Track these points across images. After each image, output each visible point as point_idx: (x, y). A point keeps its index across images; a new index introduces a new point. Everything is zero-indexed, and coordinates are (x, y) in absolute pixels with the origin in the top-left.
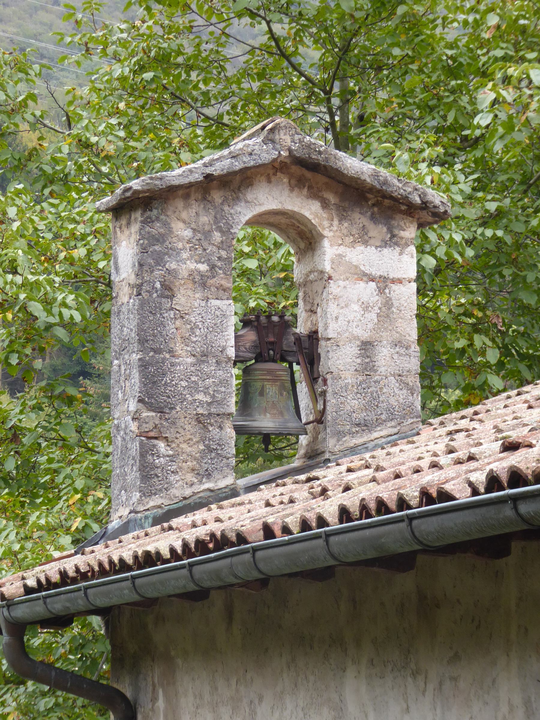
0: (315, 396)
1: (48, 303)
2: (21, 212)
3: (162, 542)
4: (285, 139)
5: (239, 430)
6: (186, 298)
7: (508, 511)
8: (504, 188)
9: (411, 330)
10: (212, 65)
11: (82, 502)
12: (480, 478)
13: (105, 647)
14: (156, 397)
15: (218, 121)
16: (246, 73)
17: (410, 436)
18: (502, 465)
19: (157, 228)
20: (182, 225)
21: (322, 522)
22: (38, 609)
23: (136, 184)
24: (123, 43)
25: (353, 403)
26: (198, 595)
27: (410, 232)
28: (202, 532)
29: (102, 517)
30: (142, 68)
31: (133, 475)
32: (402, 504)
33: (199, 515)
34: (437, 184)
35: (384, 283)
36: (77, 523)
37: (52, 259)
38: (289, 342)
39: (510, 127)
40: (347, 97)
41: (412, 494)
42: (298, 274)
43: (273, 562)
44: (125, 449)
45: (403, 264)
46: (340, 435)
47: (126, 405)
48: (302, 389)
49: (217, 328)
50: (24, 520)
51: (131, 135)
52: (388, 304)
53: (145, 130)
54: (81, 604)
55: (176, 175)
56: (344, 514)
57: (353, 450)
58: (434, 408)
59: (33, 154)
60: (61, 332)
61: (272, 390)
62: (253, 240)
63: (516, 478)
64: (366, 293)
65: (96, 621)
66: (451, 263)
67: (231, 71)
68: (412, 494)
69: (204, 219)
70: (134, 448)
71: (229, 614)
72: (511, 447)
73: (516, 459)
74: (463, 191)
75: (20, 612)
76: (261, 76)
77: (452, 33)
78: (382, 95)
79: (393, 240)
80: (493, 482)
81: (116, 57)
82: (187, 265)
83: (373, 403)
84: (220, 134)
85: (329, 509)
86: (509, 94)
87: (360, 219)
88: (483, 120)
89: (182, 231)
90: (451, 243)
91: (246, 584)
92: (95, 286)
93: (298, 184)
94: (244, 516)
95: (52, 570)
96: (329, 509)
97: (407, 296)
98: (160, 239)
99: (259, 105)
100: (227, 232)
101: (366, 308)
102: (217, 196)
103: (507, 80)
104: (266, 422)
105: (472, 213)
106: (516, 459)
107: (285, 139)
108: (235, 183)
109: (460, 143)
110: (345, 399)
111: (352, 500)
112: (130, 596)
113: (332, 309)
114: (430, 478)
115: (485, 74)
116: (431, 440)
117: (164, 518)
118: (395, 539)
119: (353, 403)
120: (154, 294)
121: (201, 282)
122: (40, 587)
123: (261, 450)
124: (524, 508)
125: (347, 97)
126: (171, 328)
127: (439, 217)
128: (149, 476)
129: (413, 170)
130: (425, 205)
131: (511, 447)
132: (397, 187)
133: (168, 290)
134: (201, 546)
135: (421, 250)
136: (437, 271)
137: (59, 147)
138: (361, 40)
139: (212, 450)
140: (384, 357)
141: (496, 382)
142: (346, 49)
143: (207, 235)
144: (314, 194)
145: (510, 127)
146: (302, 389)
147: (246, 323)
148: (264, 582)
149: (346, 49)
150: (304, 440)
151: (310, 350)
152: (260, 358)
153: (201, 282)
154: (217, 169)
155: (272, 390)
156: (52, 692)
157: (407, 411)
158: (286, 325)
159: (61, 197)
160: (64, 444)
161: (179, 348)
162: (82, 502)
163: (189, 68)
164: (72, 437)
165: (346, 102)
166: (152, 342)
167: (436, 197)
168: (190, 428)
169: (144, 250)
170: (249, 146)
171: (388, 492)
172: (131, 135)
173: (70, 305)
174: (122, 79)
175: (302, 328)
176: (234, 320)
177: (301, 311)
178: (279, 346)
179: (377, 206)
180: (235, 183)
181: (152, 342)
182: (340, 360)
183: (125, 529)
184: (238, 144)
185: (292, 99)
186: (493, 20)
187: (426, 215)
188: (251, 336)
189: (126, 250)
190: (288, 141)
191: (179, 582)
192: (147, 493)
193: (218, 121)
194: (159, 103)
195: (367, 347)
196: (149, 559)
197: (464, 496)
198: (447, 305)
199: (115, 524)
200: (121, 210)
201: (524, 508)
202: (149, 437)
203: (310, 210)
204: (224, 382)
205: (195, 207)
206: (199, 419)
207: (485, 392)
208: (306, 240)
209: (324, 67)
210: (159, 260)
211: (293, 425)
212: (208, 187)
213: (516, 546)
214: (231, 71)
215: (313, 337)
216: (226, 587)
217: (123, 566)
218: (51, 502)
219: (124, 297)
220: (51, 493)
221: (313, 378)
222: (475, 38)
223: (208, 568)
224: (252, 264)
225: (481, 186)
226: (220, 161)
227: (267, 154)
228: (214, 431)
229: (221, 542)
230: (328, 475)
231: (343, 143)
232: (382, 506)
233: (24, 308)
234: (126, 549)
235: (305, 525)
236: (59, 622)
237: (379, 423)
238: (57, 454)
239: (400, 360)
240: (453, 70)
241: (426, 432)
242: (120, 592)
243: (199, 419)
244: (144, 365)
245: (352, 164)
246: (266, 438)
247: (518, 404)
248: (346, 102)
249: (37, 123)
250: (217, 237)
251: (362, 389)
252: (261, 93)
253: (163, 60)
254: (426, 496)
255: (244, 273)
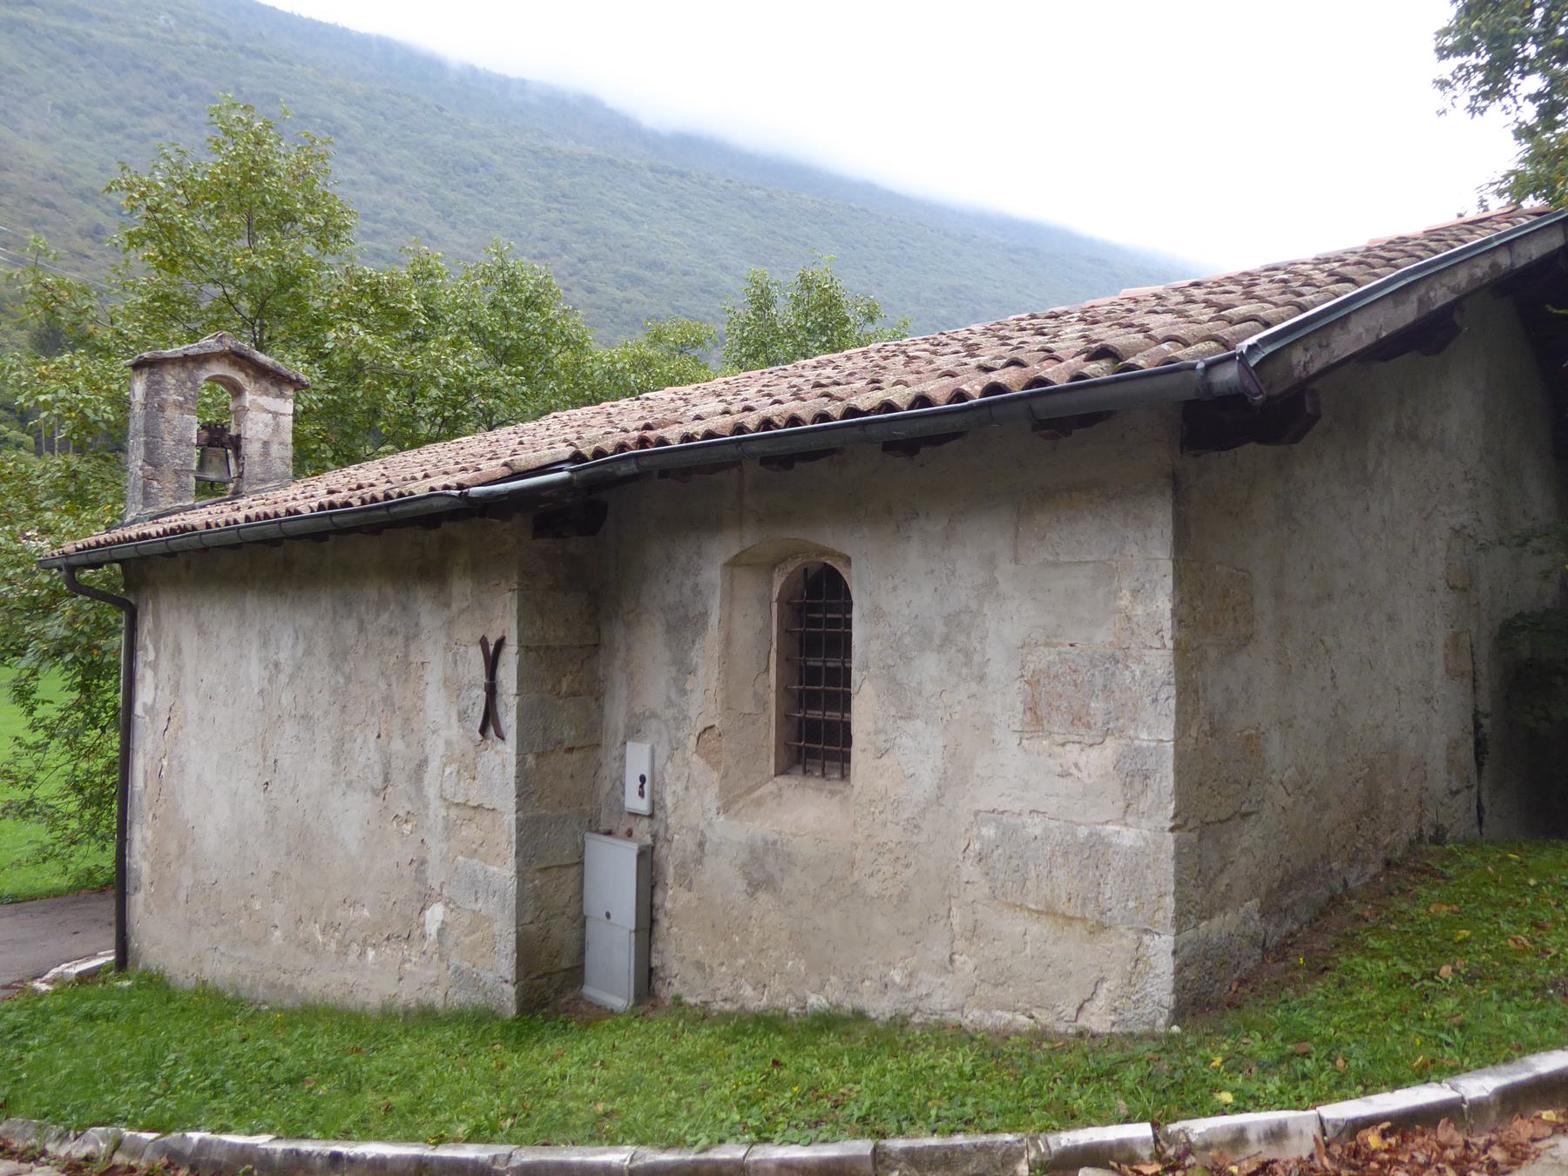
0: (238, 465)
1: (96, 411)
2: (82, 364)
3: (152, 529)
4: (228, 342)
5: (197, 479)
6: (171, 413)
7: (327, 521)
8: (338, 379)
9: (289, 438)
10: (191, 303)
11: (112, 509)
12: (315, 505)
13: (121, 580)
14: (152, 458)
15: (195, 331)
16: (210, 309)
17: (284, 487)
18: (325, 500)
19: (157, 378)
20: (170, 378)
21: (236, 522)
22: (84, 559)
23: (146, 355)
24: (144, 287)
25: (258, 470)
26: (171, 555)
27: (290, 392)
28: (173, 525)
29: (121, 517)
30: (154, 300)
31: (139, 497)
32: (277, 515)
33: (173, 518)
34: (305, 372)
35: (276, 415)
36: (108, 519)
37: (99, 389)
38: (225, 439)
39: (342, 350)
40: (263, 327)
41: (282, 511)
42: (231, 407)
43: (210, 540)
44: (135, 484)
45: (287, 407)
46: (250, 484)
47: (136, 461)
48: (232, 462)
49: (188, 428)
50: (78, 516)
51: (146, 332)
52: (278, 425)
53: (154, 331)
54: (107, 557)
55: (168, 352)
56: (247, 519)
57: (257, 492)
58: (296, 476)
59: (90, 336)
60: (102, 425)
61: (215, 461)
62: (210, 389)
63: (332, 505)
64: (266, 419)
65: (117, 566)
66: (311, 410)
67: (203, 307)
68: (282, 511)
69: (183, 375)
70: (140, 484)
71: (188, 568)
72: (331, 492)
73: (332, 498)
74: (1032, 709)
75: (73, 561)
76: (219, 311)
77: (318, 304)
78: (281, 329)
79: (281, 395)
80: (321, 507)
81: (140, 294)
82: (173, 397)
83: (268, 470)
84: (194, 336)
85: (240, 516)
86: (342, 335)
87: (265, 384)
88: (330, 345)
89: (170, 380)
90: (311, 400)
91: (196, 550)
92: (122, 403)
93: (233, 364)
94: (196, 518)
95: (92, 541)
96: (240, 516)
97: (287, 421)
98: (158, 383)
99: (216, 324)
100: (194, 382)
101: (266, 426)
102: (190, 365)
103: (342, 329)
104: (212, 476)
105: (323, 387)
106: (332, 498)
107: (228, 342)
108: (201, 360)
109: (318, 355)
110: (253, 467)
111: (252, 513)
112: (133, 554)
113: (249, 425)
114: (292, 504)
115: (331, 325)
116: (296, 489)
117: (155, 518)
118: (272, 531)
119: (258, 470)
120: (155, 409)
121: (180, 406)
122: (85, 548)
123: (208, 490)
124: (335, 519)
125: (263, 327)
126: (162, 427)
127: (305, 387)
128: (147, 498)
129: (295, 364)
130: (298, 381)
131: (331, 492)
132: (284, 370)
133: (161, 408)
134: (173, 531)
135: (296, 402)
136: (304, 413)
137: (104, 334)
138: (271, 301)
139: (182, 487)
140: (275, 449)
141: (330, 465)
142: (263, 305)
143: (184, 383)
144: (242, 369)
145: (342, 350)
146: (232, 462)
147: (203, 427)
148: (206, 549)
149: (263, 305)
150: (231, 486)
151: (236, 443)
152: (210, 445)
153: (180, 406)
154: (190, 352)
155: (215, 461)
156: (91, 601)
157: (285, 475)
158: (224, 430)
159: (107, 358)
160: (103, 481)
161: (166, 437)
162: (112, 509)
163: (180, 303)
164: (108, 477)
165: (262, 330)
166: (151, 432)
167: (304, 378)
168: (170, 476)
169: (149, 387)
170: (208, 342)
171: (269, 510)
172: (146, 332)
173: (109, 413)
174: (143, 304)
175: (233, 432)
176: (197, 426)
177: (233, 426)
178: (220, 440)
179: (276, 379)
180: (201, 360)
181: (151, 432)
182: (252, 449)
183: (134, 522)
184: (202, 342)
185: (234, 325)
186: (336, 301)
187: (298, 385)
188: (205, 434)
189: (139, 387)
190: (229, 343)
191: (162, 548)
192: (146, 506)
193: (195, 331)
194: (163, 318)
195: (266, 444)
196: (145, 536)
197: (307, 513)
198: (309, 429)
199: (128, 520)
200: (138, 366)
201: (335, 519)
202: (148, 480)
203: (239, 377)
204: (190, 455)
205: (178, 370)
206: (176, 472)
207: (325, 469)
208: (237, 391)
209: (251, 312)
210: (157, 393)
211: (226, 478)
212: (185, 360)
213: (331, 537)
214: (203, 307)
215: (239, 437)
216: (184, 551)
217: (131, 539)
218: (94, 508)
219: (137, 409)
220: (95, 503)
221: (238, 456)
222: (327, 307)
223: (176, 542)
224: (209, 400)
225: (328, 375)
226: (192, 349)
227: (218, 348)
228: (184, 479)
229: (183, 530)
230: (242, 502)
231: (260, 348)
232: (266, 516)
233: (82, 411)
234: (133, 532)
235: (227, 523)
236: (96, 565)
237: (271, 480)
238: (99, 485)
239: (283, 451)
240: (315, 322)
241: (294, 486)
242: (129, 552)
243: (176, 472)
244: (146, 443)
245: (262, 357)
246: (212, 484)
247: (339, 475)
248: (262, 330)
249: (94, 320)
250: (189, 384)
251: (263, 463)
252: (218, 320)
253: (166, 298)
254: (288, 512)
255: (205, 404)
